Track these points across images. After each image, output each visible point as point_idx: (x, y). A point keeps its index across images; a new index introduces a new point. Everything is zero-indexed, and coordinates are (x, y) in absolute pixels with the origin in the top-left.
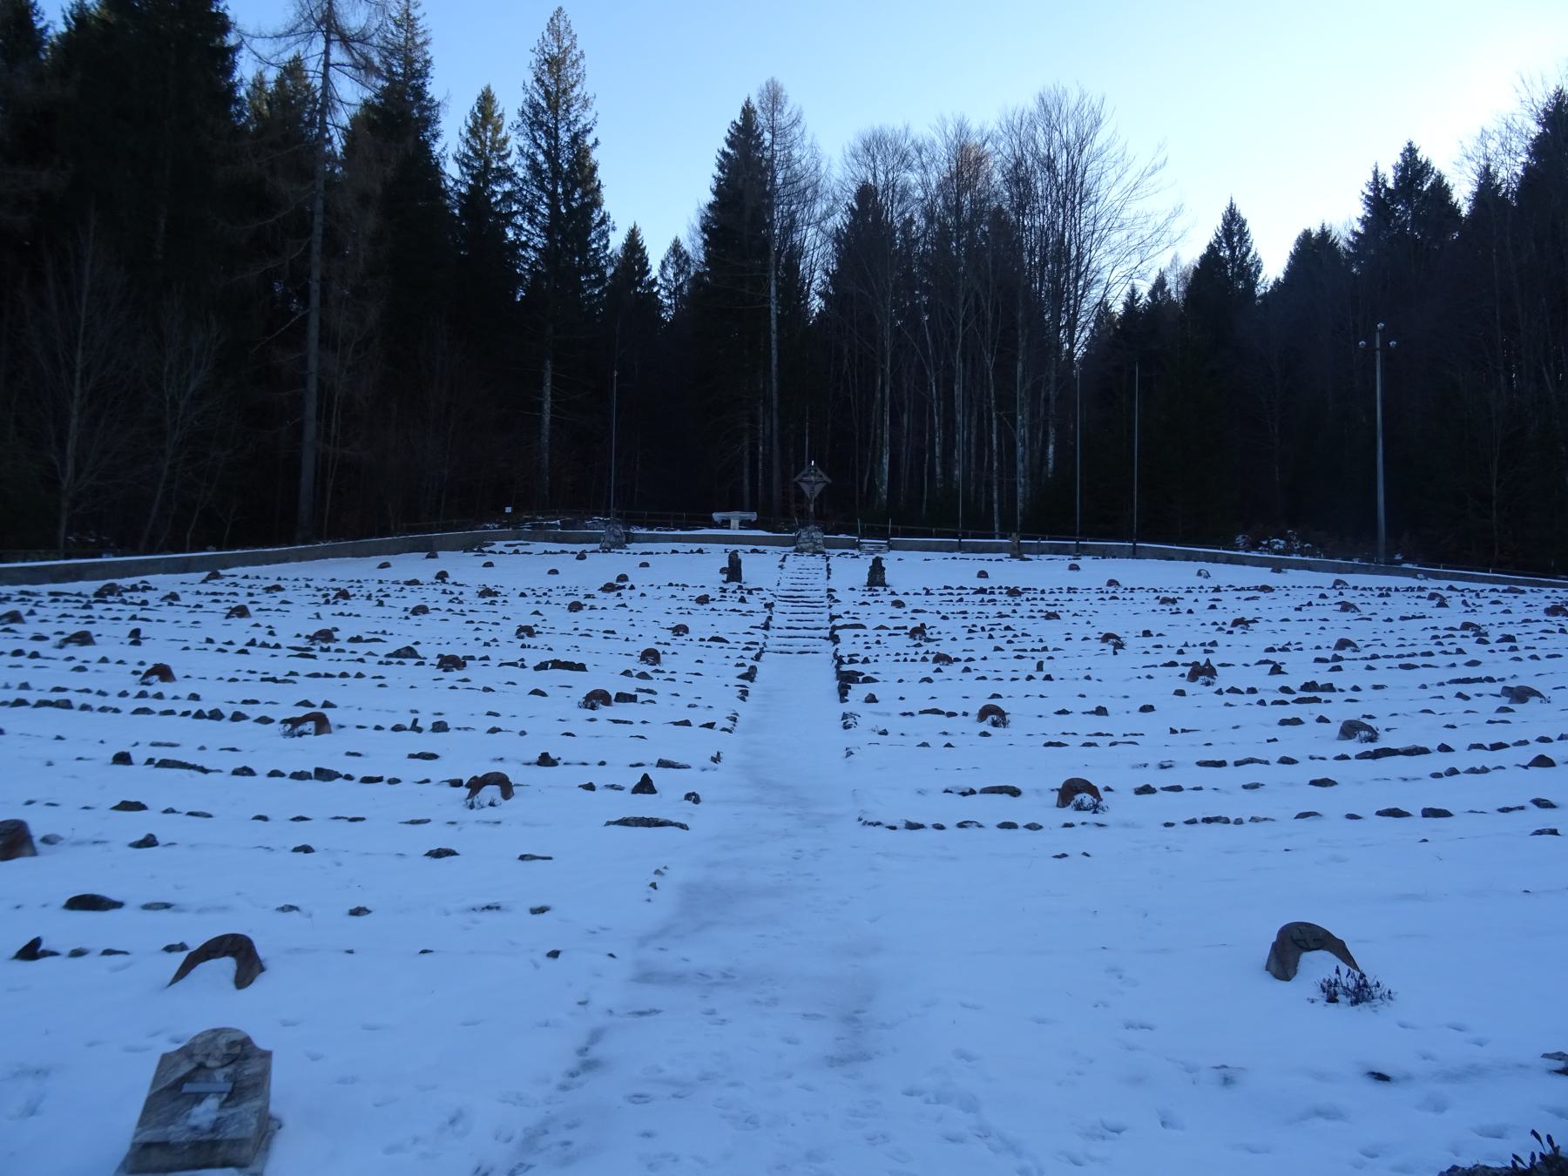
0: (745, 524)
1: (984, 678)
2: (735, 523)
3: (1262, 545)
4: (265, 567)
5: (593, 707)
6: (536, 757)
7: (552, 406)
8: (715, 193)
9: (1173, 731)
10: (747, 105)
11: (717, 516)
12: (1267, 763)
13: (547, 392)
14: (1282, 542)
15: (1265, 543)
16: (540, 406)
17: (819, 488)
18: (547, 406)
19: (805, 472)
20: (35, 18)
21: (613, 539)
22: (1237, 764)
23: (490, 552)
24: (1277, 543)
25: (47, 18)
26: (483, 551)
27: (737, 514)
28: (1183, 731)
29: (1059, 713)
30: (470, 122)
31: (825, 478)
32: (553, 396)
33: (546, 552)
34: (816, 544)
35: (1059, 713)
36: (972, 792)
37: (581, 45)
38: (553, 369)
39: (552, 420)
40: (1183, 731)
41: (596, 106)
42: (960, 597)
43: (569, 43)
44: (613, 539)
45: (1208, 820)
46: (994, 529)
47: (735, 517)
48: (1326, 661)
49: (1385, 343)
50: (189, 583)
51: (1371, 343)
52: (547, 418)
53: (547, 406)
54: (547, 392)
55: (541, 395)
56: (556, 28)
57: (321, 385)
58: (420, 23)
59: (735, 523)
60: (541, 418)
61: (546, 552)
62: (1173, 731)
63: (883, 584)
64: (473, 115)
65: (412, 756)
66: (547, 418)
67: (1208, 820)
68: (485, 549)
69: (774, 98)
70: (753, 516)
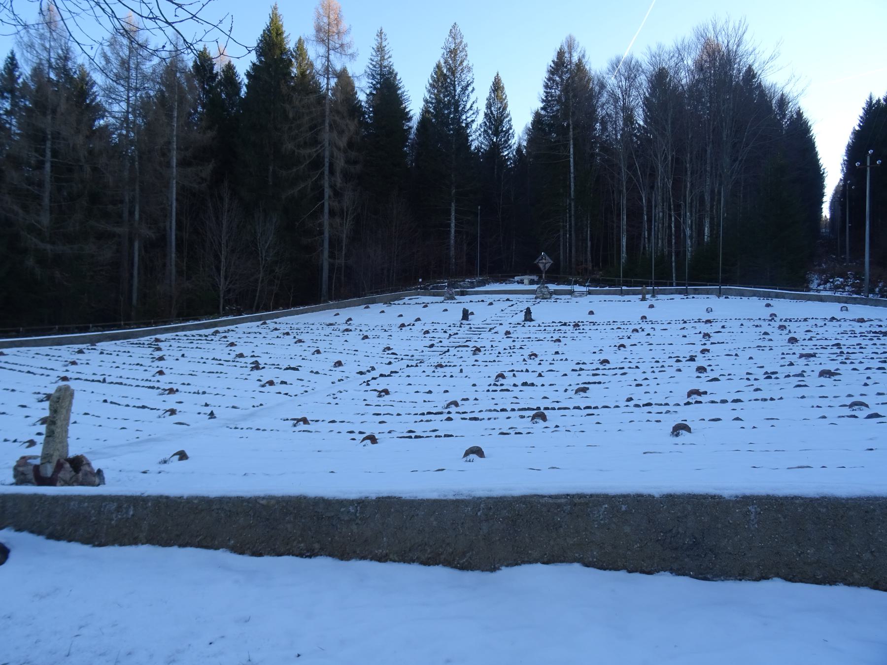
0: (532, 282)
1: (428, 376)
2: (526, 281)
3: (829, 281)
4: (285, 318)
5: (704, 354)
6: (204, 404)
7: (455, 224)
8: (543, 101)
9: (425, 401)
10: (560, 50)
11: (517, 278)
12: (392, 415)
13: (453, 218)
14: (841, 280)
15: (831, 280)
16: (449, 226)
17: (548, 266)
18: (453, 225)
19: (540, 258)
20: (237, 78)
21: (449, 296)
22: (384, 415)
23: (394, 304)
24: (838, 280)
25: (241, 77)
26: (391, 304)
27: (527, 277)
28: (429, 401)
29: (416, 392)
30: (431, 81)
31: (550, 261)
32: (456, 219)
33: (416, 303)
34: (544, 294)
35: (416, 392)
36: (287, 420)
37: (465, 41)
38: (456, 206)
39: (456, 231)
40: (429, 401)
41: (474, 70)
42: (440, 340)
43: (454, 45)
44: (449, 296)
45: (304, 431)
46: (673, 280)
47: (526, 279)
48: (576, 370)
49: (873, 162)
50: (253, 326)
51: (863, 162)
52: (453, 231)
53: (453, 225)
54: (453, 218)
55: (450, 220)
56: (454, 33)
57: (220, 275)
58: (386, 49)
59: (526, 281)
60: (450, 231)
61: (416, 303)
62: (425, 401)
63: (531, 320)
64: (432, 77)
65: (177, 402)
66: (453, 231)
67: (304, 431)
68: (392, 303)
69: (571, 44)
70: (535, 278)
